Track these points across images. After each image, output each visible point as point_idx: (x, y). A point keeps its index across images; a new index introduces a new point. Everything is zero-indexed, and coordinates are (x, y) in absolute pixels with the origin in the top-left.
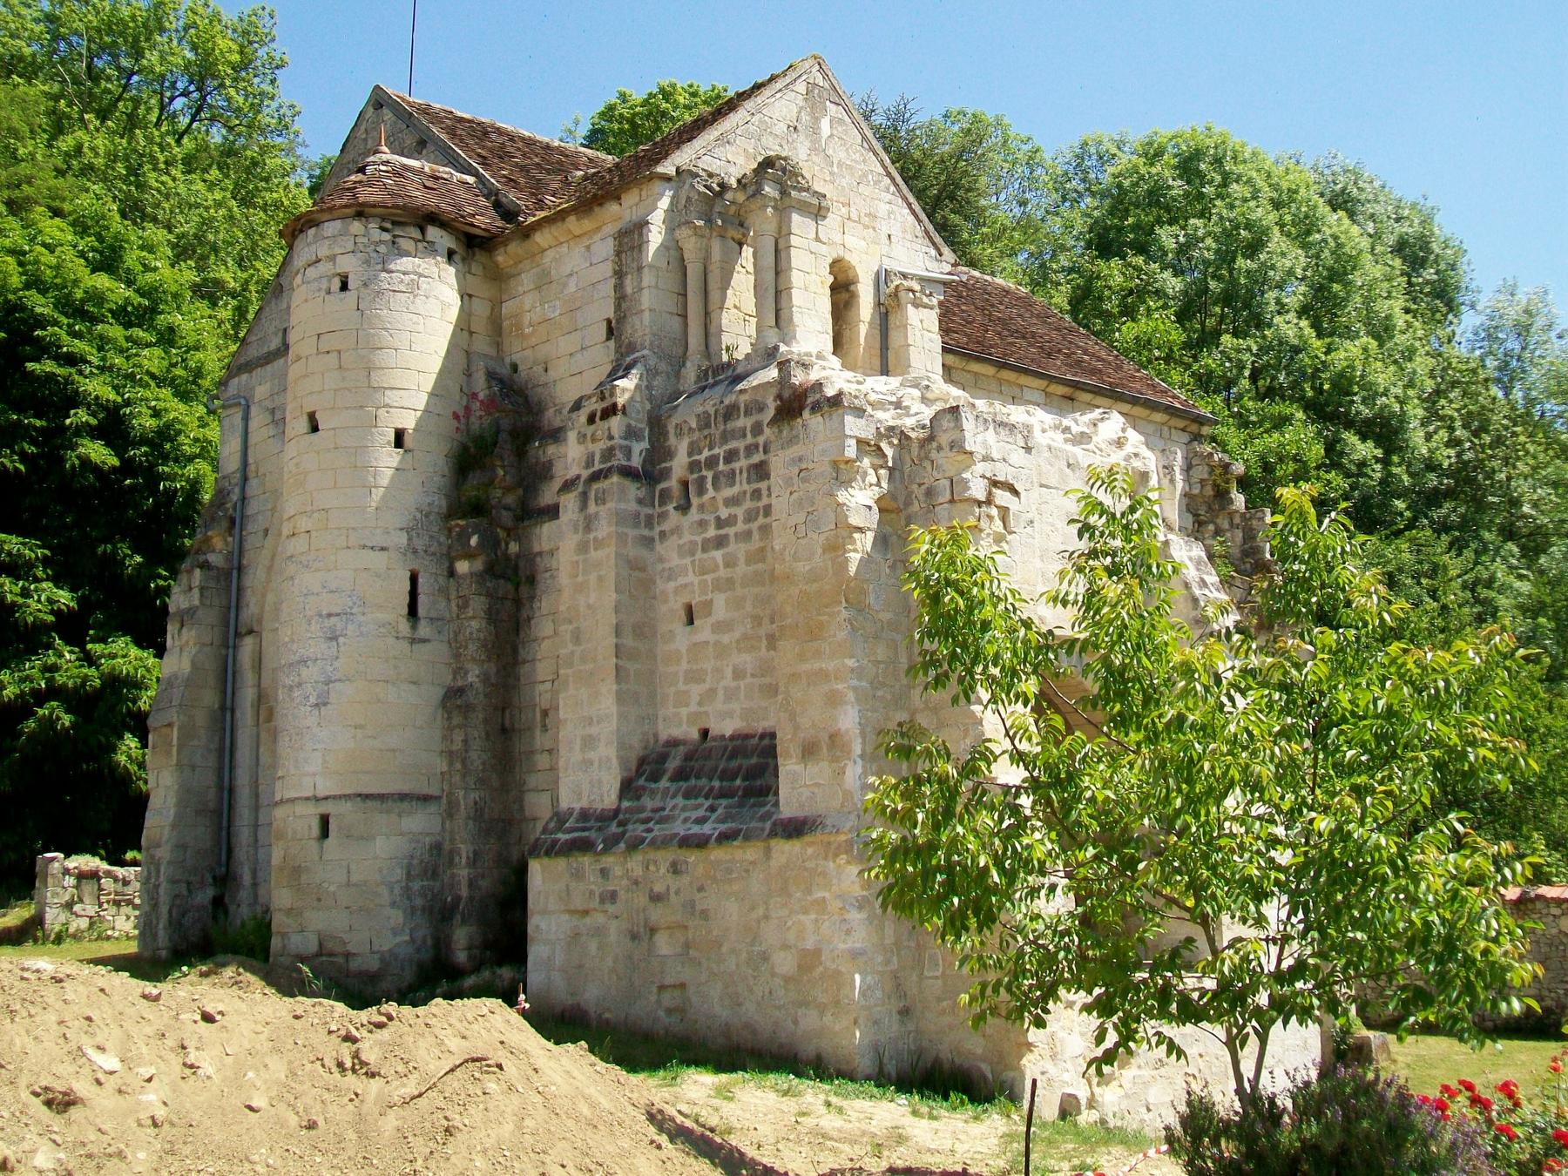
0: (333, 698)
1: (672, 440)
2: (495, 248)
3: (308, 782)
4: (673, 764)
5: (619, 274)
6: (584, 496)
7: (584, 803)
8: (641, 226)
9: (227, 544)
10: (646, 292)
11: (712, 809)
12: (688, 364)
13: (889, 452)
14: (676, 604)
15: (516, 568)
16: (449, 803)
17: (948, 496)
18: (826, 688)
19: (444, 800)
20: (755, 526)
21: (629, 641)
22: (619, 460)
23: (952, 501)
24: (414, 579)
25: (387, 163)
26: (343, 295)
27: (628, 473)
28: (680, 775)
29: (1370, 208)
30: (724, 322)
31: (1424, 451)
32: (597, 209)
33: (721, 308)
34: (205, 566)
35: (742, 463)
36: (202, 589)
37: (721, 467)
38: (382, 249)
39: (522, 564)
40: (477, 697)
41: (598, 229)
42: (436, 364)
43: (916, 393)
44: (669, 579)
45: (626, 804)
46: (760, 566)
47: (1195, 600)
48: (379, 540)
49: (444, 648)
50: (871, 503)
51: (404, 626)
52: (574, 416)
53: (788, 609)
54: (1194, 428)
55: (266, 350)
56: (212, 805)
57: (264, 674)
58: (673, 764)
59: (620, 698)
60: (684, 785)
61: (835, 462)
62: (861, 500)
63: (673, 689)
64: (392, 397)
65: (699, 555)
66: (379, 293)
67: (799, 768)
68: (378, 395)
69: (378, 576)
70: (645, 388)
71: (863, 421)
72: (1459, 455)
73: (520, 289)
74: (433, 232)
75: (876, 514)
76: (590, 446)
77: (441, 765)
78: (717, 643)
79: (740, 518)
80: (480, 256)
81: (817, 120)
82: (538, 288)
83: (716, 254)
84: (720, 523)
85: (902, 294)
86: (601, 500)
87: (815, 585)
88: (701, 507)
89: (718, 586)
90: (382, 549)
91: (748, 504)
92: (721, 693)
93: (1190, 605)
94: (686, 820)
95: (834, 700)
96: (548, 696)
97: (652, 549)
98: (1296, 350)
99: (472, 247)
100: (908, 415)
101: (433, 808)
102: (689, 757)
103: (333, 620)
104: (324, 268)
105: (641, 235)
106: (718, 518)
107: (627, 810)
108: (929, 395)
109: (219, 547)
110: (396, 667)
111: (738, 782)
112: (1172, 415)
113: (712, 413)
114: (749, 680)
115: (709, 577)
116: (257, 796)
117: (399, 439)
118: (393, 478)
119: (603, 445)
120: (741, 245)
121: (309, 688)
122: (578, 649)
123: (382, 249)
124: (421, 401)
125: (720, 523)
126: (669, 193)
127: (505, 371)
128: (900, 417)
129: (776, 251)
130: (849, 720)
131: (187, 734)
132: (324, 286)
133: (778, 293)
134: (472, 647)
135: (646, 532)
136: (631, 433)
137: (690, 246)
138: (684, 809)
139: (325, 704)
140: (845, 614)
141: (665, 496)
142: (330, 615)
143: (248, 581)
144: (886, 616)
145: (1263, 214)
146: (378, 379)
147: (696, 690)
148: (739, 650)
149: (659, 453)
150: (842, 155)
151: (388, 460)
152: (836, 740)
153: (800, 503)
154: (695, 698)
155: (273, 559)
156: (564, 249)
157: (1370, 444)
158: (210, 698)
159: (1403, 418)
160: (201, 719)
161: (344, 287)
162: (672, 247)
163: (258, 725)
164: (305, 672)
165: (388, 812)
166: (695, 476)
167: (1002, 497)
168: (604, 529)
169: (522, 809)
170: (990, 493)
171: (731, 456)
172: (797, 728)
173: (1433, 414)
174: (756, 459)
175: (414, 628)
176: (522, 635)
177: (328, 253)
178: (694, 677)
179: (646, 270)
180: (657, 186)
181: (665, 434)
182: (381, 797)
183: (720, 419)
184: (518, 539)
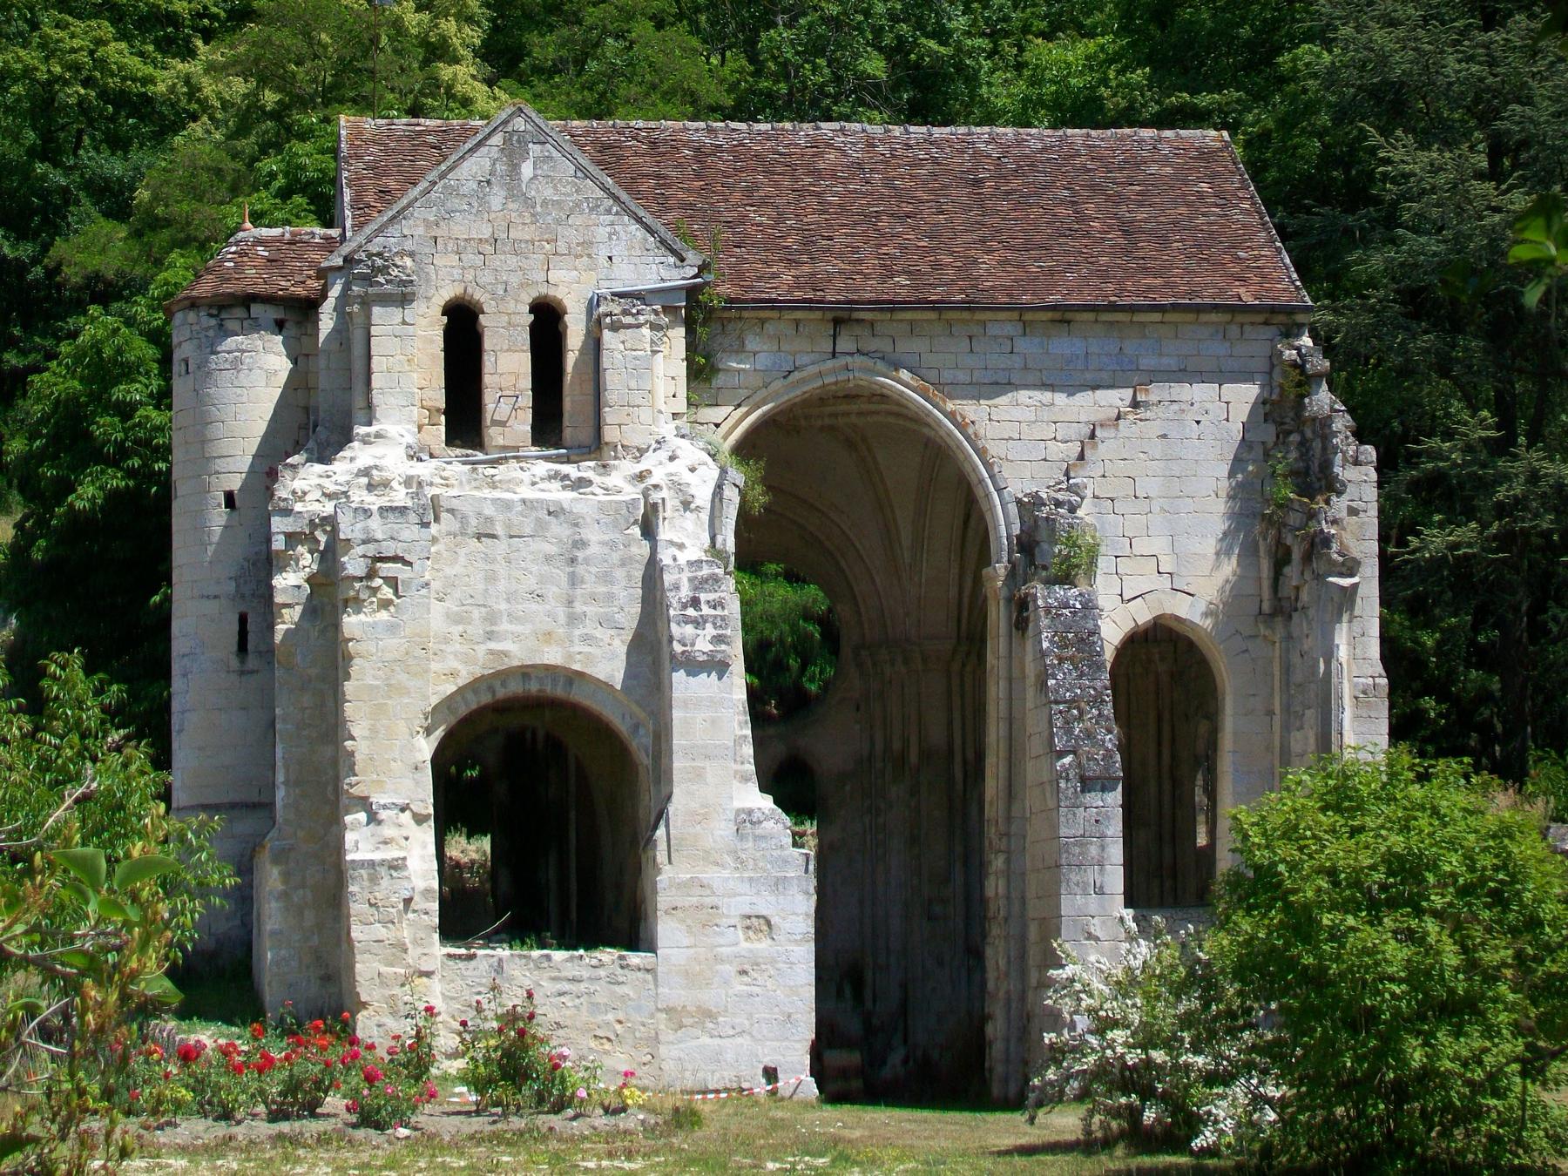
24: (243, 620)
38: (211, 333)
42: (261, 427)
50: (301, 582)
51: (234, 663)
64: (220, 465)
66: (209, 374)
71: (291, 519)
74: (256, 309)
90: (216, 597)
117: (230, 499)
144: (313, 672)
175: (243, 662)
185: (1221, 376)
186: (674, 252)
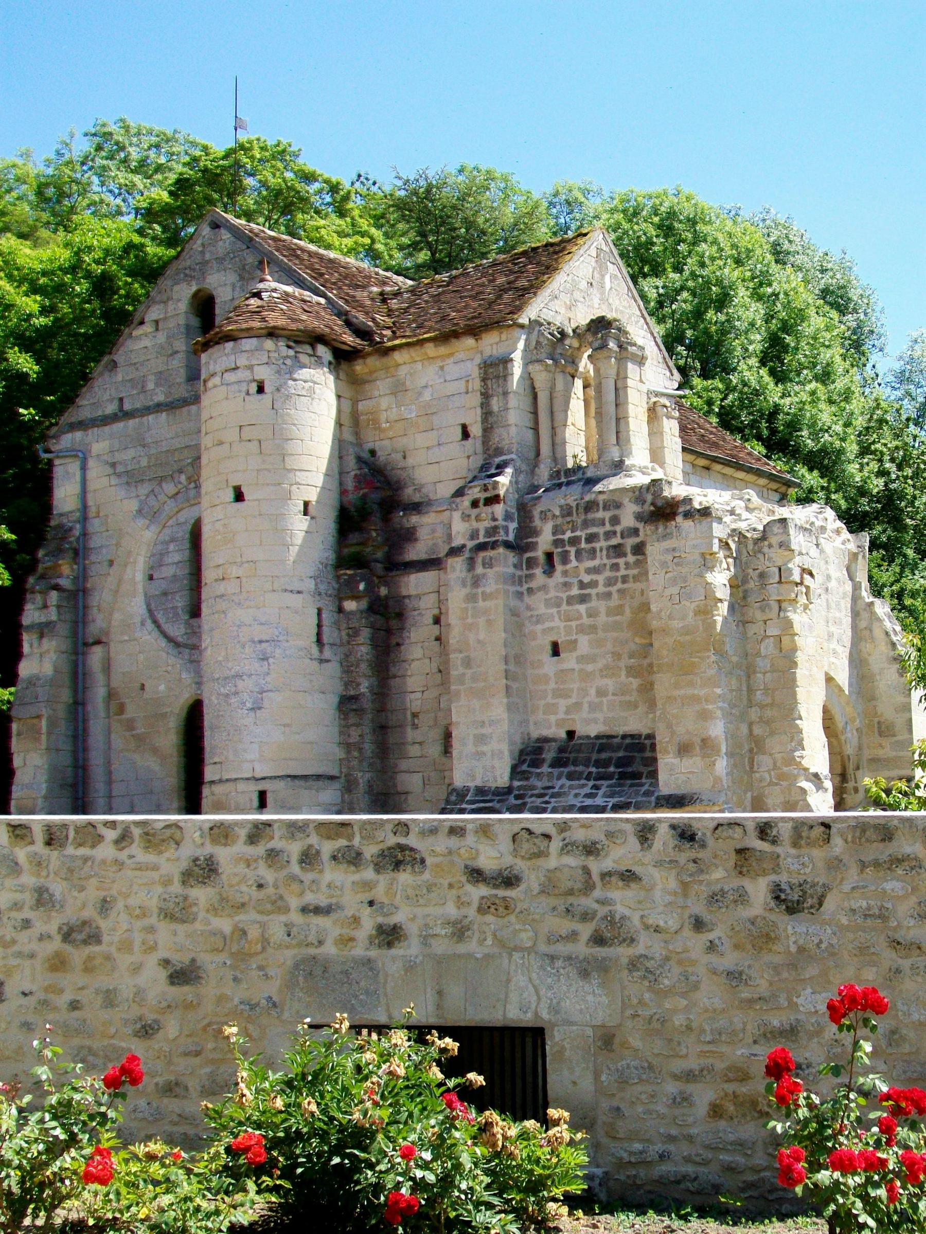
0: (266, 704)
1: (537, 522)
2: (355, 359)
3: (247, 766)
4: (549, 755)
5: (486, 396)
6: (471, 563)
7: (479, 783)
8: (506, 361)
9: (73, 570)
10: (511, 412)
11: (596, 787)
12: (542, 466)
13: (733, 546)
14: (545, 643)
15: (386, 607)
16: (348, 781)
17: (777, 579)
18: (697, 708)
19: (343, 780)
20: (614, 589)
21: (512, 667)
22: (501, 536)
23: (780, 582)
24: (319, 614)
25: (275, 290)
26: (260, 396)
27: (508, 545)
28: (558, 763)
29: (799, 259)
30: (567, 435)
31: (857, 479)
32: (454, 340)
33: (565, 425)
34: (57, 587)
35: (602, 544)
36: (59, 607)
37: (583, 545)
38: (288, 362)
39: (391, 603)
40: (367, 703)
41: (452, 354)
43: (742, 504)
44: (538, 622)
45: (516, 784)
46: (618, 618)
47: (893, 645)
48: (297, 586)
49: (338, 665)
51: (315, 650)
52: (458, 500)
53: (665, 653)
54: (783, 489)
55: (100, 413)
56: (70, 781)
57: (113, 674)
58: (549, 755)
59: (510, 708)
60: (566, 770)
61: (703, 555)
62: (720, 578)
63: (542, 702)
64: (300, 477)
65: (564, 607)
66: (288, 397)
67: (676, 761)
68: (291, 475)
69: (296, 613)
70: (515, 482)
72: (886, 485)
73: (376, 393)
74: (322, 350)
75: (728, 590)
76: (475, 524)
77: (340, 753)
78: (581, 670)
79: (601, 583)
80: (344, 366)
81: (603, 276)
82: (393, 394)
83: (560, 385)
84: (582, 585)
85: (659, 409)
86: (488, 564)
87: (688, 638)
88: (565, 573)
89: (581, 630)
90: (299, 592)
91: (608, 573)
92: (586, 706)
93: (890, 647)
94: (576, 795)
95: (705, 716)
96: (419, 703)
97: (522, 601)
98: (757, 393)
99: (343, 358)
100: (740, 520)
101: (337, 785)
102: (561, 750)
103: (264, 645)
104: (241, 375)
105: (506, 368)
106: (581, 582)
107: (519, 788)
108: (751, 506)
109: (66, 570)
110: (311, 681)
111: (612, 769)
112: (771, 480)
113: (574, 504)
114: (610, 697)
115: (574, 624)
116: (110, 773)
118: (304, 539)
119: (487, 524)
120: (573, 377)
121: (245, 696)
122: (469, 672)
123: (288, 362)
124: (319, 480)
125: (582, 585)
126: (524, 337)
127: (366, 455)
128: (735, 521)
129: (616, 389)
130: (717, 729)
131: (52, 724)
132: (244, 389)
133: (618, 420)
134: (364, 666)
135: (519, 589)
136: (508, 517)
137: (541, 379)
138: (571, 787)
139: (260, 708)
140: (713, 658)
141: (531, 563)
142: (261, 642)
143: (94, 600)
144: (735, 659)
145: (731, 273)
146: (290, 463)
147: (563, 703)
148: (602, 676)
149: (526, 531)
150: (617, 302)
151: (299, 525)
152: (707, 744)
153: (674, 581)
154: (562, 709)
155: (118, 586)
156: (419, 366)
157: (816, 473)
158: (66, 695)
159: (841, 452)
160: (61, 711)
161: (261, 390)
162: (529, 380)
163: (108, 717)
164: (240, 684)
165: (310, 788)
166: (559, 550)
167: (807, 579)
168: (490, 586)
169: (395, 786)
170: (802, 578)
171: (591, 538)
172: (673, 733)
173: (865, 450)
174: (614, 541)
175: (321, 651)
176: (392, 655)
177: (247, 363)
178: (561, 693)
179: (511, 395)
180: (517, 332)
181: (531, 518)
182: (305, 777)
183: (581, 510)
184: (387, 584)
185: (626, 368)
186: (671, 371)
